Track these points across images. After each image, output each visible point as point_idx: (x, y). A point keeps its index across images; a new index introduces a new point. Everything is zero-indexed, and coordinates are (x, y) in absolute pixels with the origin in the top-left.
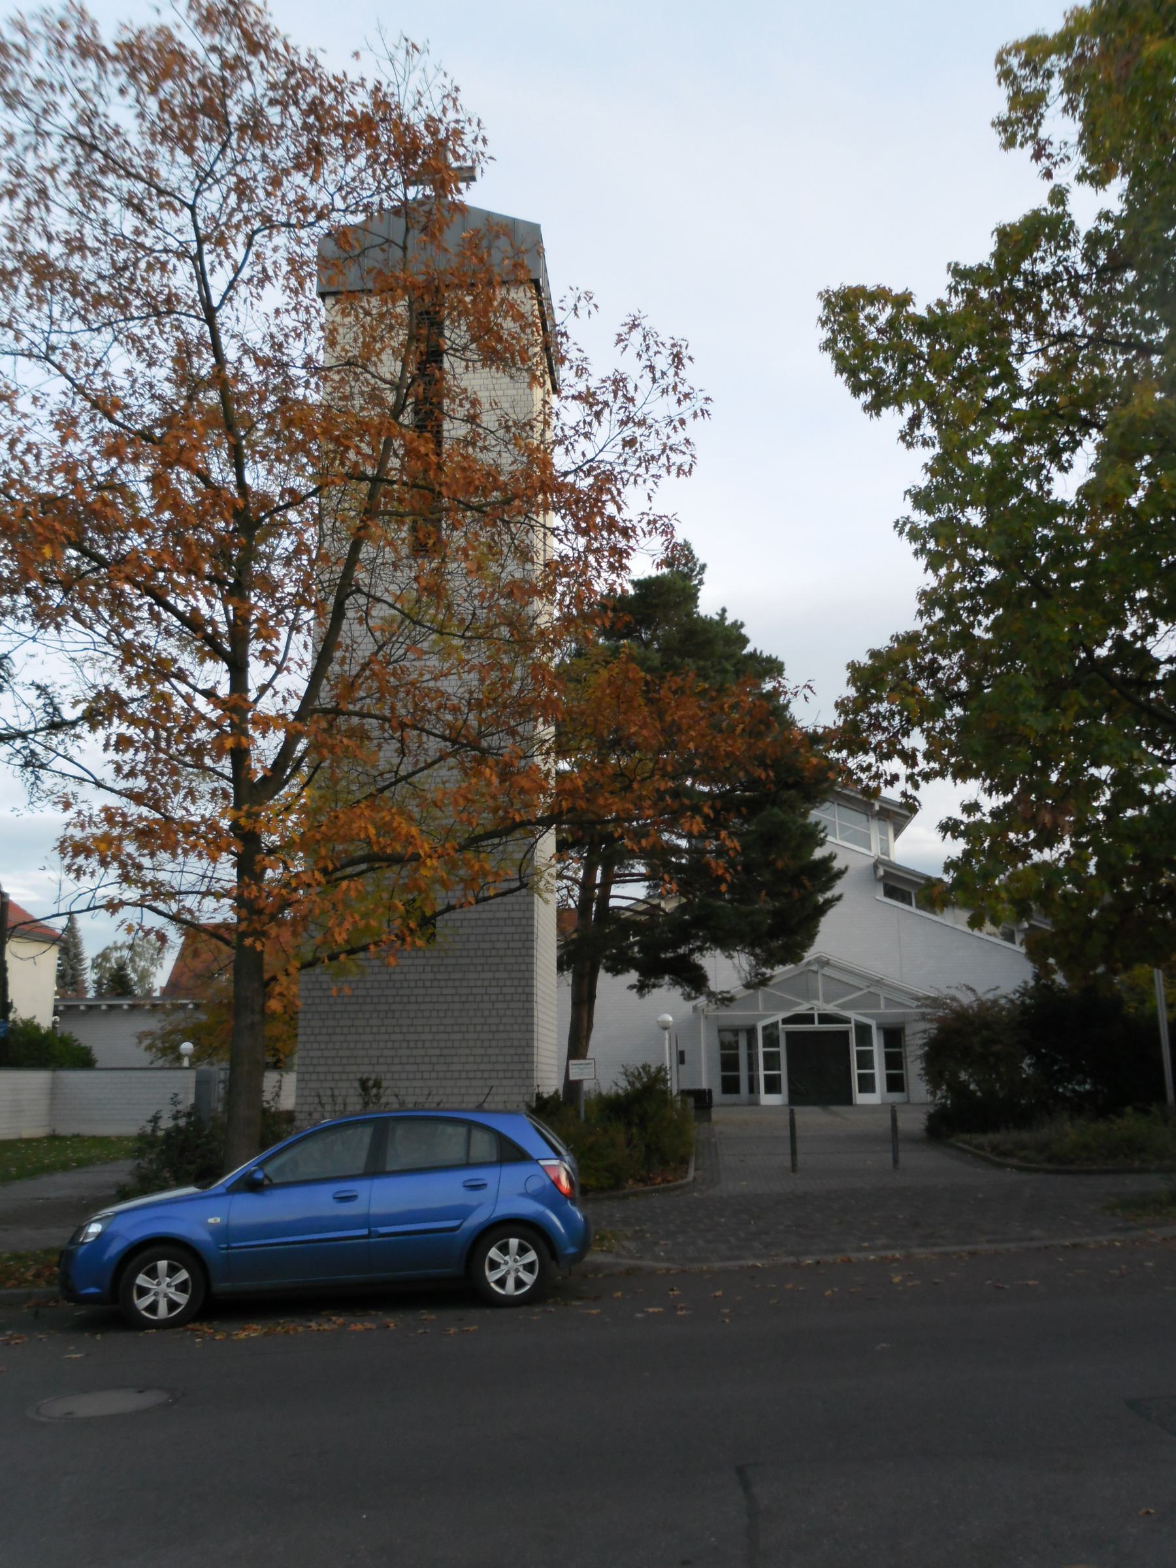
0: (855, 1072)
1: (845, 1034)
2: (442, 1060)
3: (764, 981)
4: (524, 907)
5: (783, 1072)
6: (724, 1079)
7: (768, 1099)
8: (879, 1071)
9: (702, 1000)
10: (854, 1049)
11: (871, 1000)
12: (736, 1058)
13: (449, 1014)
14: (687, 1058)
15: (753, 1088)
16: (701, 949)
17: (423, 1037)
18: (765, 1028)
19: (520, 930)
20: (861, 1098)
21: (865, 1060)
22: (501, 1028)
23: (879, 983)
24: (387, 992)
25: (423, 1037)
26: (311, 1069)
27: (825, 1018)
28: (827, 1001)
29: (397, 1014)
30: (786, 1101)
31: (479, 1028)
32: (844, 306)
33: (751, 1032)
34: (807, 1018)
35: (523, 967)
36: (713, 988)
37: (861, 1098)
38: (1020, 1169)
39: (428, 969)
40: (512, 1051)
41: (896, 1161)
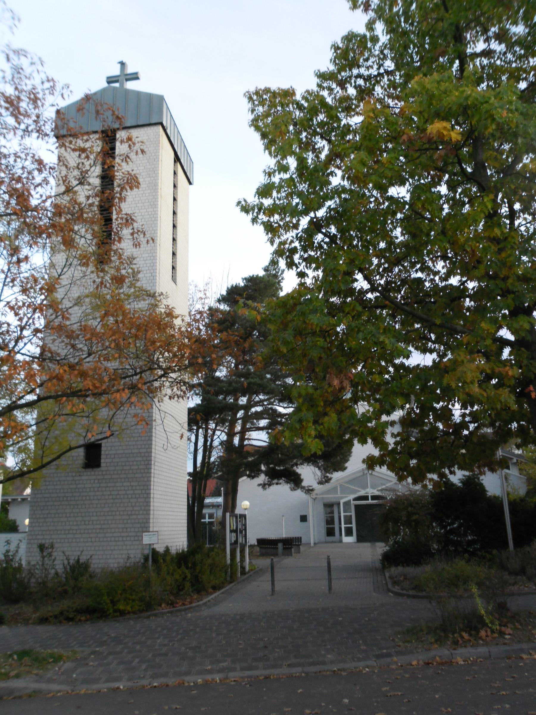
2: (102, 531)
3: (328, 480)
4: (147, 446)
5: (354, 526)
6: (327, 528)
7: (347, 540)
9: (299, 491)
12: (332, 519)
13: (106, 505)
15: (341, 534)
16: (297, 465)
17: (93, 518)
19: (145, 459)
22: (133, 512)
24: (75, 494)
25: (93, 518)
26: (34, 537)
27: (374, 498)
29: (80, 507)
30: (355, 540)
31: (122, 513)
32: (261, 97)
33: (339, 504)
34: (365, 498)
35: (146, 479)
38: (397, 594)
39: (96, 481)
40: (138, 525)
41: (330, 588)
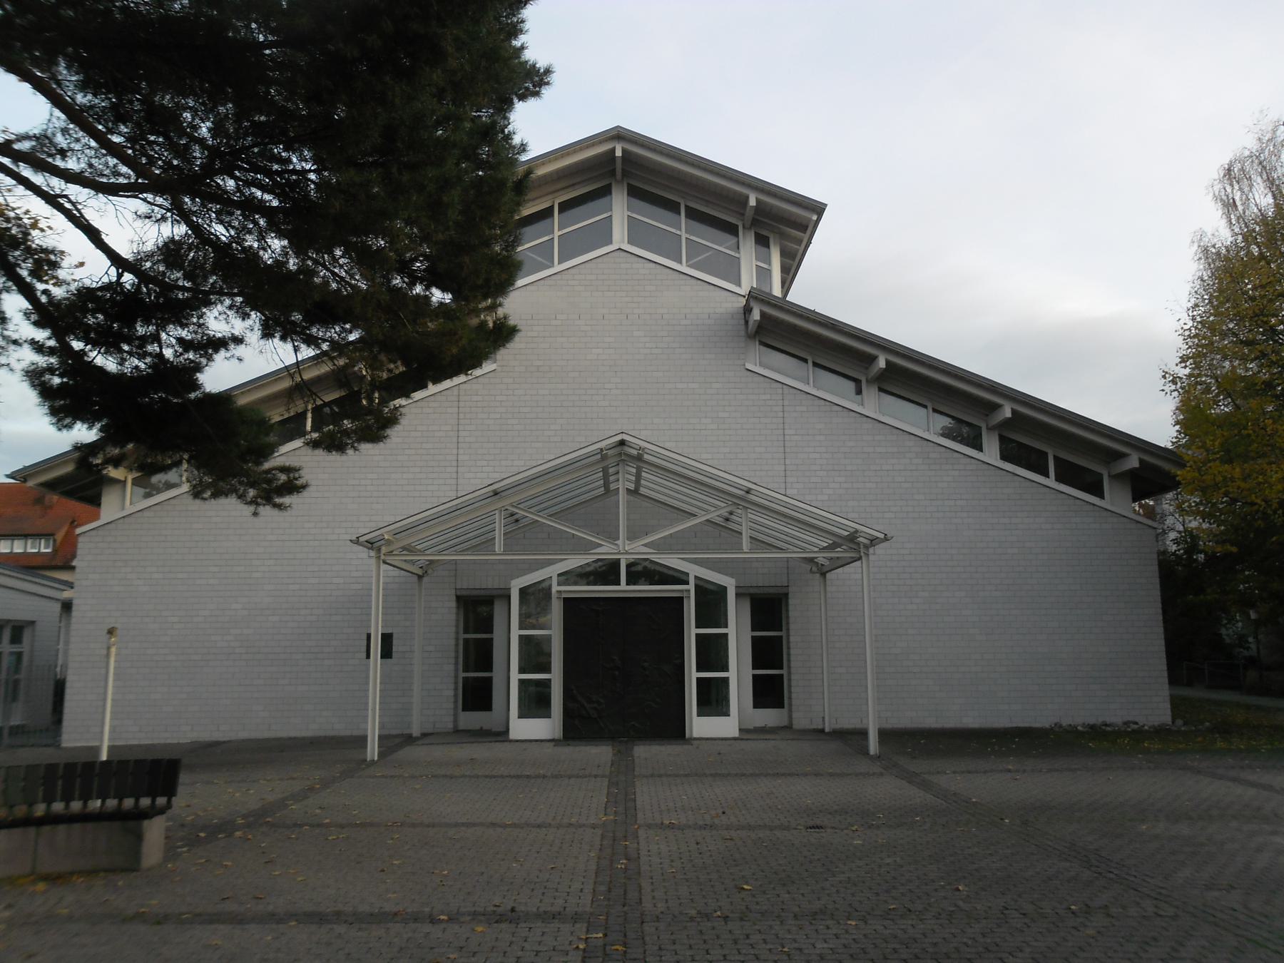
0: (693, 675)
1: (679, 602)
8: (738, 673)
10: (692, 632)
11: (724, 529)
14: (397, 646)
18: (523, 592)
20: (701, 726)
21: (713, 653)
23: (742, 499)
27: (641, 572)
28: (632, 536)
30: (558, 733)
34: (607, 572)
36: (121, 503)
37: (701, 726)
